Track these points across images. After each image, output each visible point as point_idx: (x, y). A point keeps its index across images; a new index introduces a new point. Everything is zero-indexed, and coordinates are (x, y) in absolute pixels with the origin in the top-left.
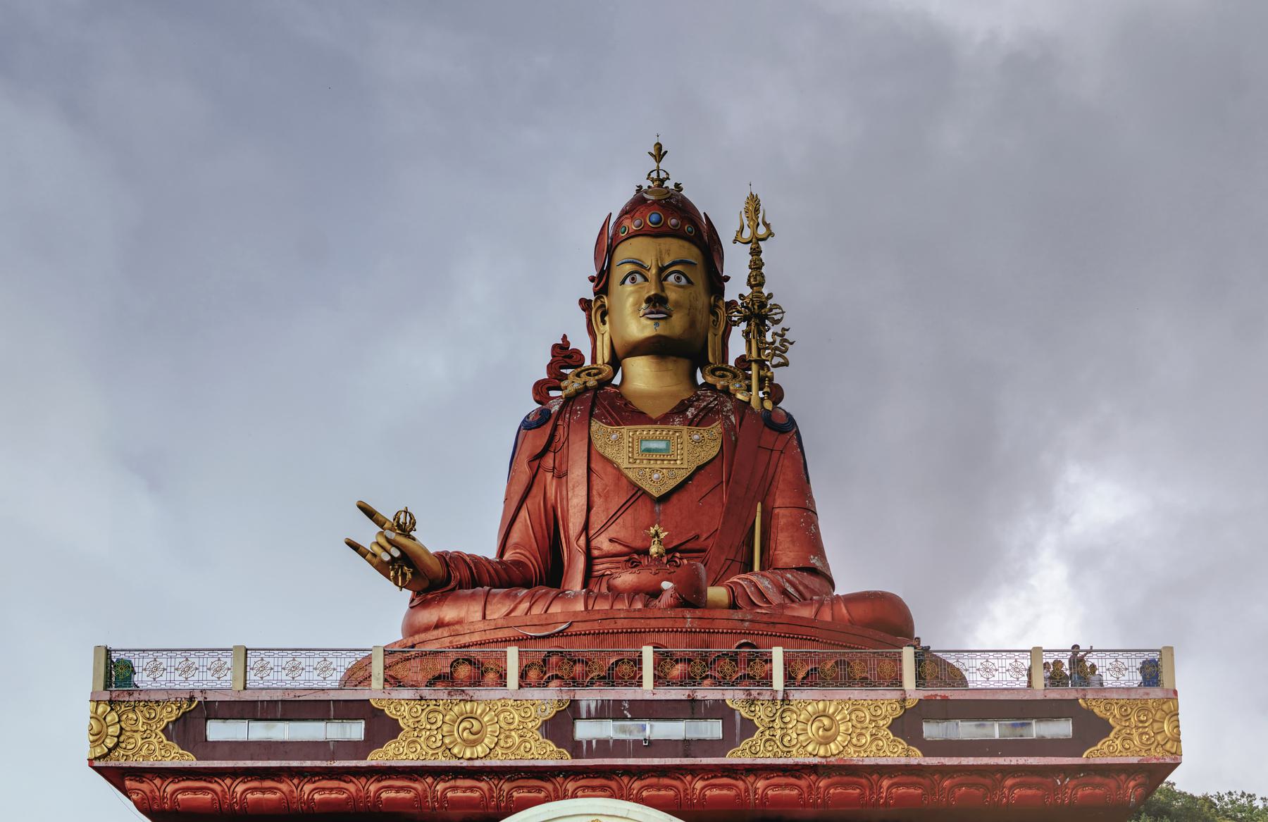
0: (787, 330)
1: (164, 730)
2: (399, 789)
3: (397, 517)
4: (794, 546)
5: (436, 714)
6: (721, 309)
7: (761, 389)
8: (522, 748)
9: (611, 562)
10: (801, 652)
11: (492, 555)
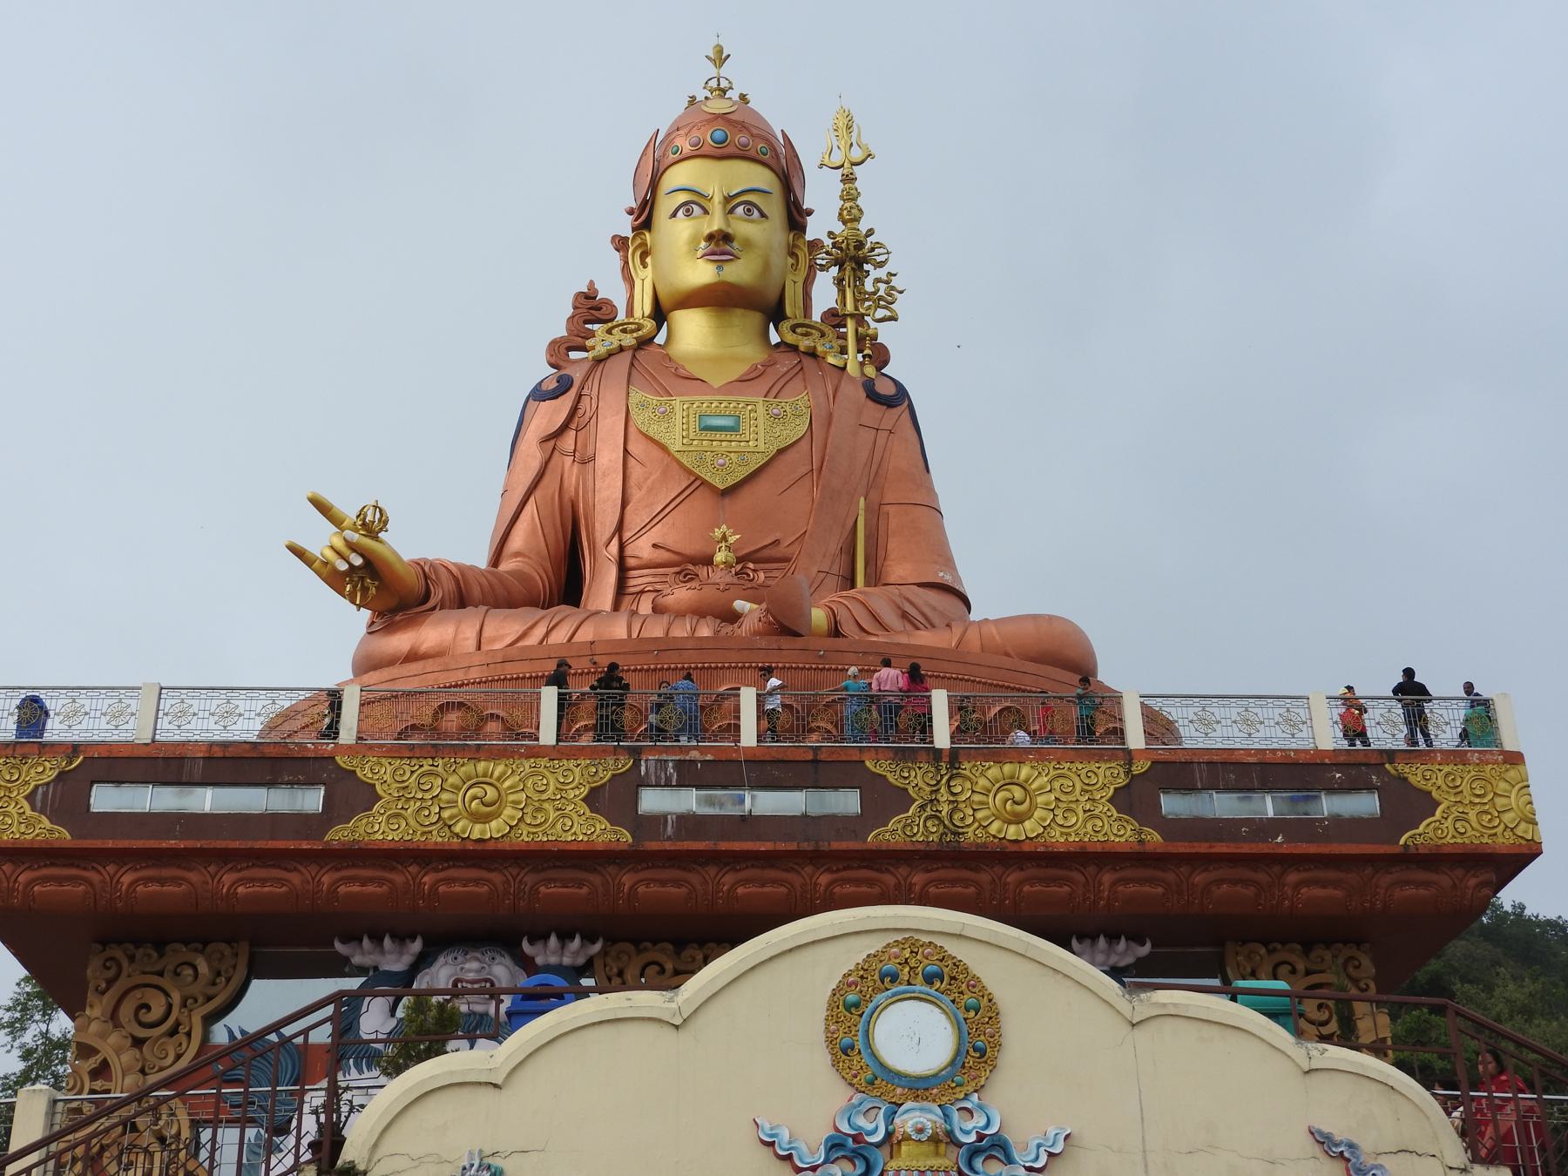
0: (895, 275)
1: (30, 798)
2: (364, 882)
3: (361, 514)
5: (432, 779)
6: (802, 250)
7: (860, 351)
8: (559, 826)
9: (655, 575)
10: (607, 694)
11: (481, 560)
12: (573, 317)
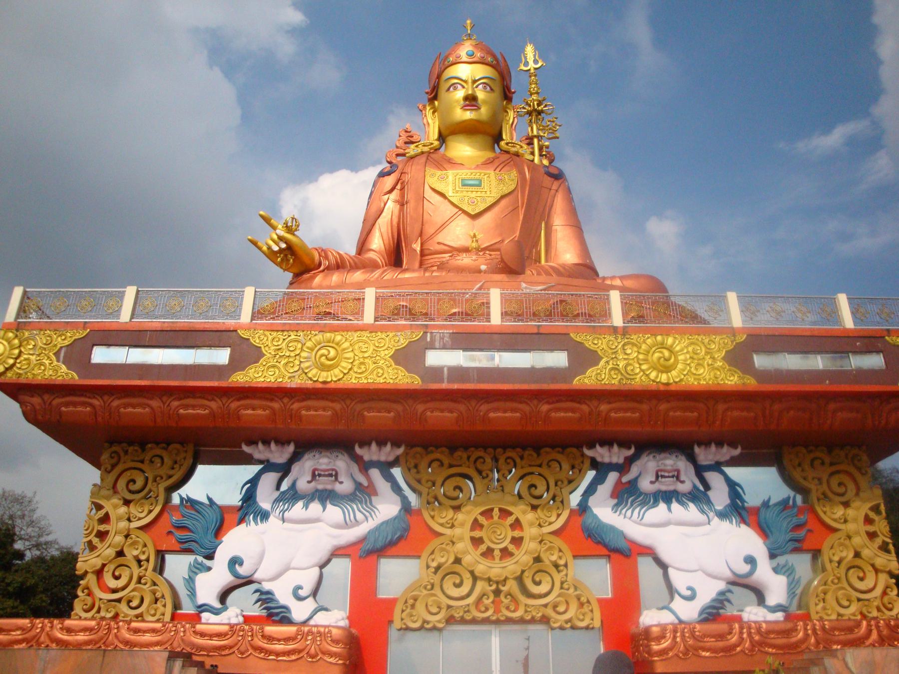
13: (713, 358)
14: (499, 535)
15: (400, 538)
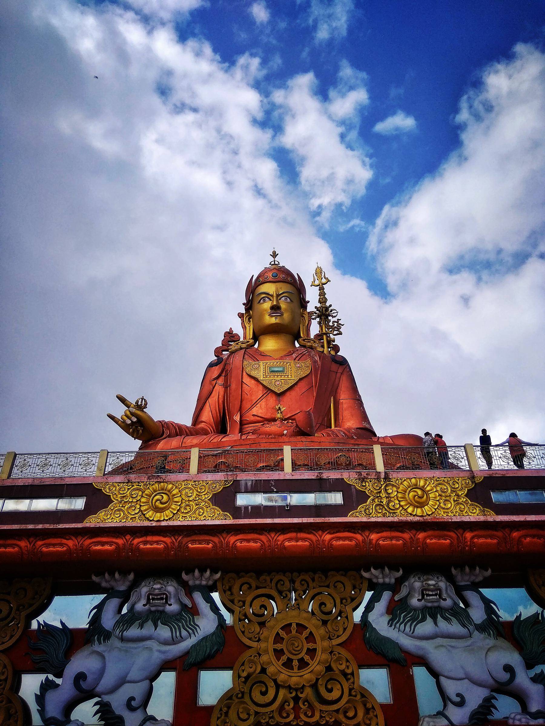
0: (340, 320)
3: (137, 402)
4: (353, 417)
12: (224, 340)
13: (458, 495)
14: (296, 647)
15: (217, 651)
